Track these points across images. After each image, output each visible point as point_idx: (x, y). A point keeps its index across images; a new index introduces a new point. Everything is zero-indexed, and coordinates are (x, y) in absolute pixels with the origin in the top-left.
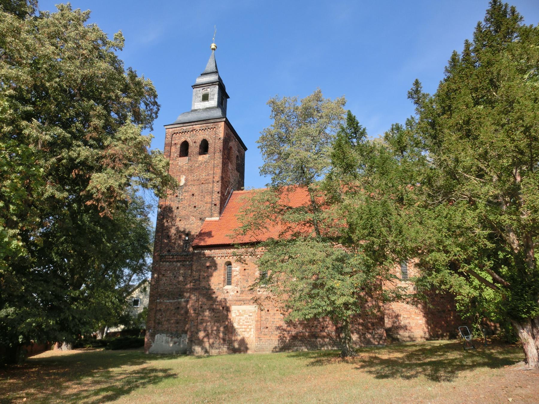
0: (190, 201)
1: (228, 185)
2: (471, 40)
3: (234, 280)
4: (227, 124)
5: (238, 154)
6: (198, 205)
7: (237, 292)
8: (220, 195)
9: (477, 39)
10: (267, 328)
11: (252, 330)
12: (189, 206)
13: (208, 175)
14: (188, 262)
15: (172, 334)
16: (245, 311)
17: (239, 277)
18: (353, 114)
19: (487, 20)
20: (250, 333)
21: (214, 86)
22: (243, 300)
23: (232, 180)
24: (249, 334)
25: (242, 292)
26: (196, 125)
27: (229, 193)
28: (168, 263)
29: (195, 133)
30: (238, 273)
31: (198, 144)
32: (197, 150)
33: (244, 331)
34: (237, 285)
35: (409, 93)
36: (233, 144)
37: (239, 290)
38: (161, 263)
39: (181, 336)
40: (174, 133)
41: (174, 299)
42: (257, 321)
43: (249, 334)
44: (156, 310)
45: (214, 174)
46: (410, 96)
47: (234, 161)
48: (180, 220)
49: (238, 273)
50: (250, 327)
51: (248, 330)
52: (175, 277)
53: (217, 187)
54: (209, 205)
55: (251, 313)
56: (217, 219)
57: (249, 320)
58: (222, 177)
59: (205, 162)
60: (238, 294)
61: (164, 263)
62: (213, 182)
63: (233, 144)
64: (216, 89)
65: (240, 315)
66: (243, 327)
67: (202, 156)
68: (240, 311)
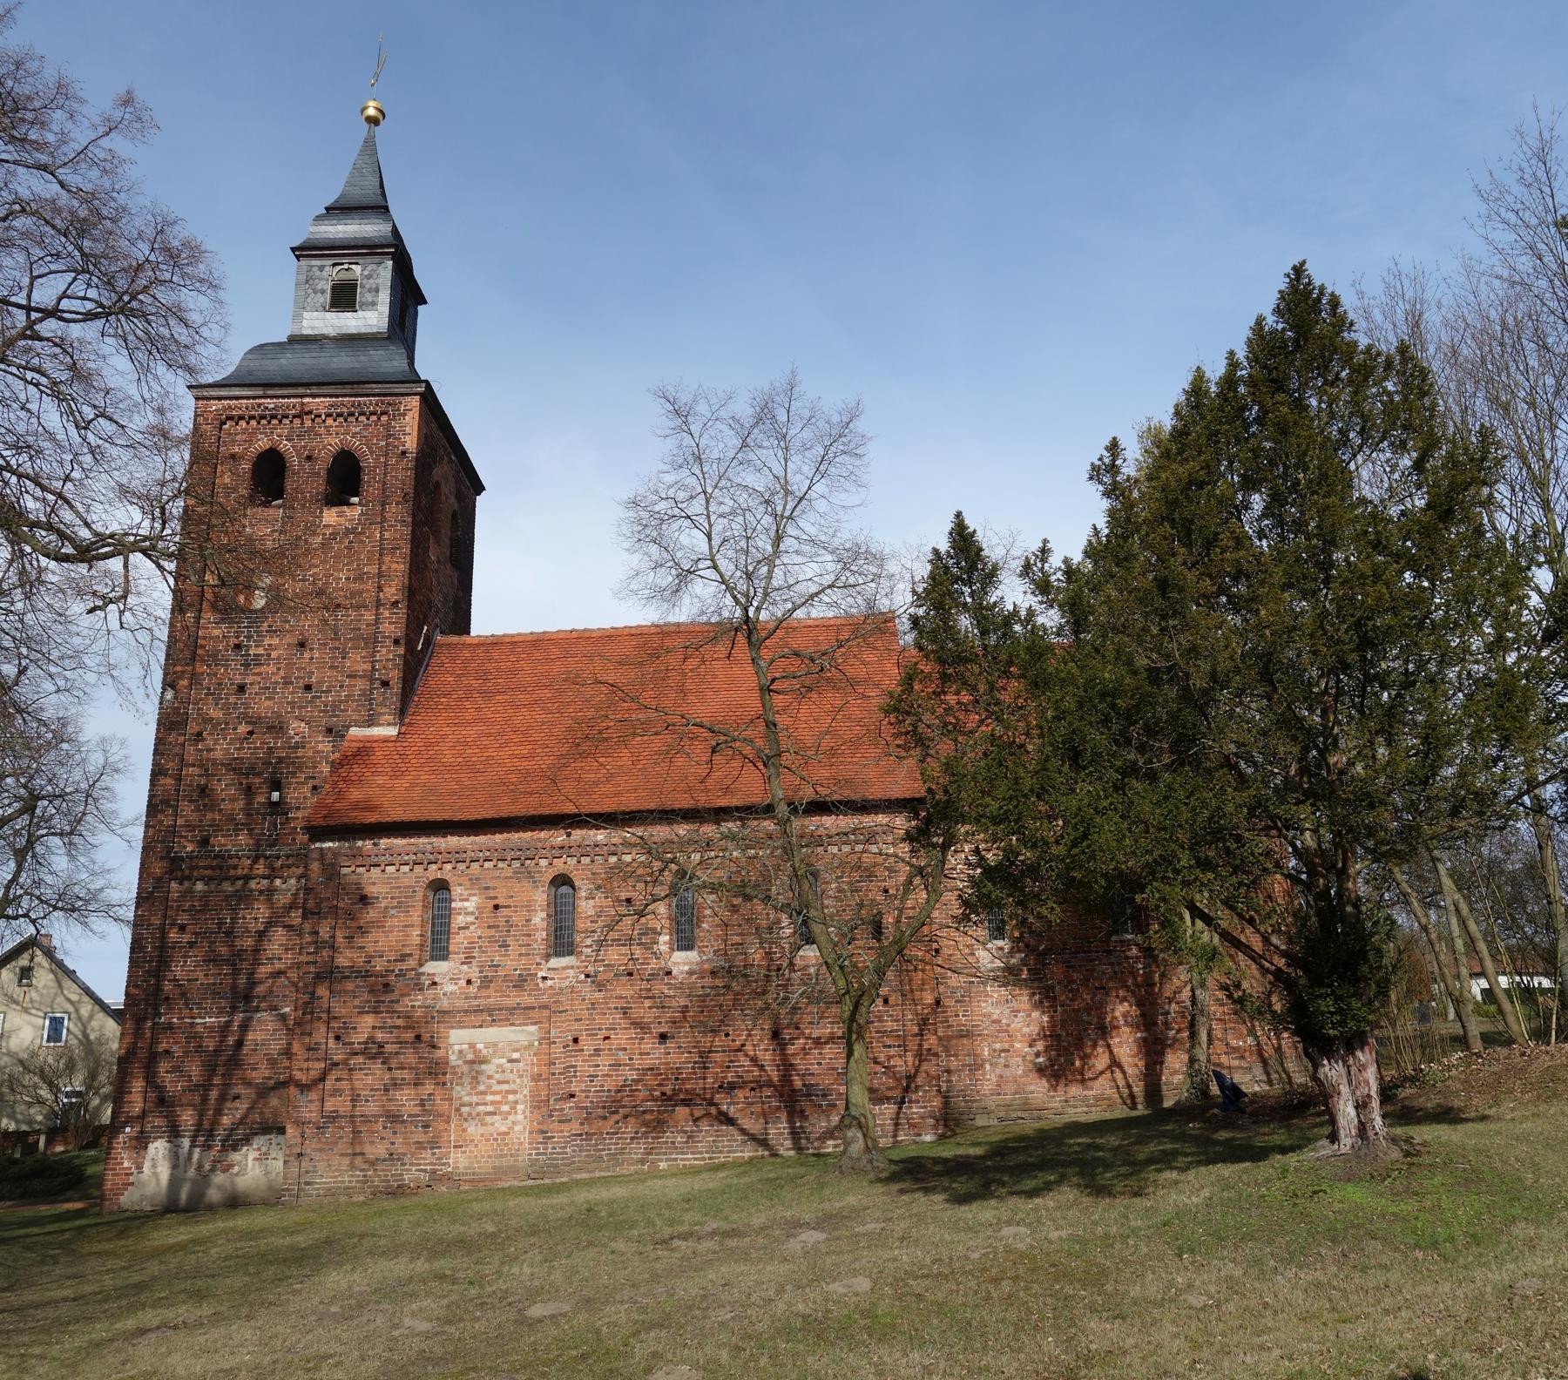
0: (290, 665)
1: (426, 617)
2: (1241, 354)
3: (458, 941)
4: (429, 406)
5: (456, 506)
6: (321, 683)
7: (469, 982)
8: (401, 651)
9: (1254, 359)
10: (572, 1096)
11: (520, 1107)
12: (287, 683)
13: (359, 578)
18: (971, 523)
19: (1277, 311)
20: (511, 1118)
21: (376, 259)
22: (490, 1011)
23: (437, 600)
24: (509, 1123)
25: (486, 982)
26: (314, 396)
27: (428, 642)
29: (308, 423)
30: (471, 919)
31: (321, 467)
32: (319, 486)
33: (494, 1113)
34: (468, 960)
35: (1094, 467)
37: (474, 973)
40: (230, 418)
42: (536, 1078)
43: (509, 1123)
45: (380, 575)
46: (1095, 473)
47: (446, 531)
49: (471, 919)
50: (511, 1097)
51: (506, 1108)
53: (392, 625)
54: (361, 684)
55: (516, 1050)
56: (392, 731)
58: (410, 587)
59: (348, 532)
60: (473, 989)
62: (379, 604)
63: (443, 471)
64: (384, 272)
67: (334, 510)
68: (480, 1046)
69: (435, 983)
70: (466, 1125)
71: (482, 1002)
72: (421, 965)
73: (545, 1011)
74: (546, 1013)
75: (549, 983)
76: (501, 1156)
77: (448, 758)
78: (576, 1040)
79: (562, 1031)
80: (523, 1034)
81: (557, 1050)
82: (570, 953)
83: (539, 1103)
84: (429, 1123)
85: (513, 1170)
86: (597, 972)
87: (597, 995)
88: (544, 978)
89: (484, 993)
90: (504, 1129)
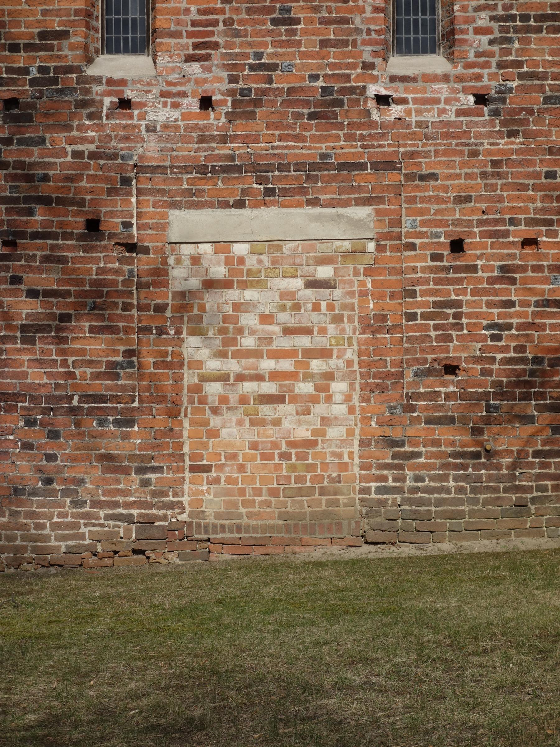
7: (206, 103)
10: (451, 369)
11: (339, 387)
16: (274, 246)
20: (320, 409)
22: (259, 170)
24: (314, 420)
25: (246, 105)
34: (201, 52)
37: (218, 85)
42: (374, 324)
43: (314, 420)
50: (317, 365)
51: (306, 388)
55: (324, 261)
60: (216, 120)
66: (267, 365)
69: (125, 104)
70: (215, 422)
71: (239, 149)
72: (90, 61)
73: (377, 175)
74: (391, 179)
75: (396, 110)
76: (300, 492)
78: (457, 246)
79: (425, 222)
80: (350, 223)
81: (420, 263)
82: (430, 48)
83: (378, 381)
84: (142, 400)
85: (327, 524)
86: (504, 91)
87: (503, 143)
88: (382, 100)
89: (242, 128)
90: (303, 433)
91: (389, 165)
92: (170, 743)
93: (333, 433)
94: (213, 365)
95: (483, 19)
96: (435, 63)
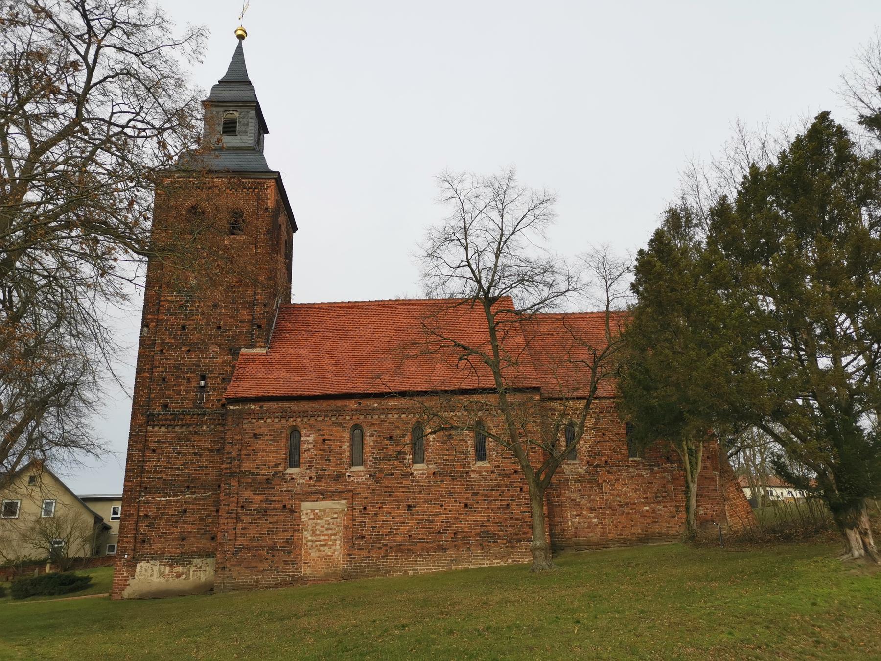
3: (305, 457)
6: (225, 325)
7: (311, 478)
10: (363, 537)
11: (338, 542)
14: (204, 428)
15: (171, 558)
16: (324, 510)
17: (313, 452)
20: (334, 548)
22: (321, 493)
24: (332, 550)
25: (319, 479)
28: (163, 429)
33: (324, 546)
34: (310, 467)
36: (282, 219)
38: (149, 428)
39: (190, 563)
41: (175, 495)
44: (139, 517)
48: (189, 351)
50: (333, 537)
51: (331, 543)
52: (178, 454)
54: (246, 326)
55: (335, 513)
57: (331, 526)
60: (313, 482)
61: (156, 428)
65: (317, 517)
66: (322, 537)
69: (293, 479)
71: (317, 488)
73: (349, 494)
74: (351, 494)
75: (352, 479)
77: (294, 365)
78: (365, 509)
81: (357, 513)
90: (330, 553)
91: (350, 491)
92: (7, 71)
93: (337, 553)
94: (310, 538)
95: (371, 458)
96: (361, 468)
